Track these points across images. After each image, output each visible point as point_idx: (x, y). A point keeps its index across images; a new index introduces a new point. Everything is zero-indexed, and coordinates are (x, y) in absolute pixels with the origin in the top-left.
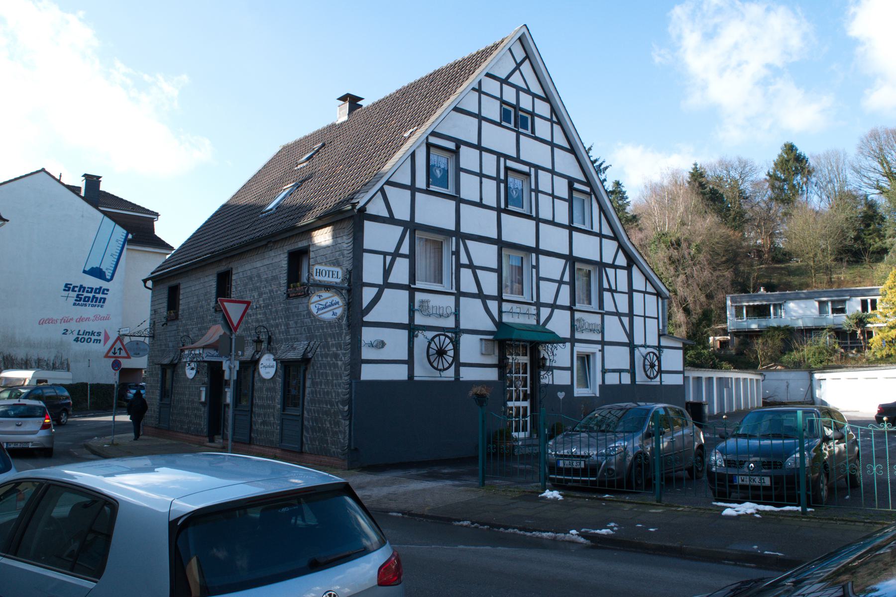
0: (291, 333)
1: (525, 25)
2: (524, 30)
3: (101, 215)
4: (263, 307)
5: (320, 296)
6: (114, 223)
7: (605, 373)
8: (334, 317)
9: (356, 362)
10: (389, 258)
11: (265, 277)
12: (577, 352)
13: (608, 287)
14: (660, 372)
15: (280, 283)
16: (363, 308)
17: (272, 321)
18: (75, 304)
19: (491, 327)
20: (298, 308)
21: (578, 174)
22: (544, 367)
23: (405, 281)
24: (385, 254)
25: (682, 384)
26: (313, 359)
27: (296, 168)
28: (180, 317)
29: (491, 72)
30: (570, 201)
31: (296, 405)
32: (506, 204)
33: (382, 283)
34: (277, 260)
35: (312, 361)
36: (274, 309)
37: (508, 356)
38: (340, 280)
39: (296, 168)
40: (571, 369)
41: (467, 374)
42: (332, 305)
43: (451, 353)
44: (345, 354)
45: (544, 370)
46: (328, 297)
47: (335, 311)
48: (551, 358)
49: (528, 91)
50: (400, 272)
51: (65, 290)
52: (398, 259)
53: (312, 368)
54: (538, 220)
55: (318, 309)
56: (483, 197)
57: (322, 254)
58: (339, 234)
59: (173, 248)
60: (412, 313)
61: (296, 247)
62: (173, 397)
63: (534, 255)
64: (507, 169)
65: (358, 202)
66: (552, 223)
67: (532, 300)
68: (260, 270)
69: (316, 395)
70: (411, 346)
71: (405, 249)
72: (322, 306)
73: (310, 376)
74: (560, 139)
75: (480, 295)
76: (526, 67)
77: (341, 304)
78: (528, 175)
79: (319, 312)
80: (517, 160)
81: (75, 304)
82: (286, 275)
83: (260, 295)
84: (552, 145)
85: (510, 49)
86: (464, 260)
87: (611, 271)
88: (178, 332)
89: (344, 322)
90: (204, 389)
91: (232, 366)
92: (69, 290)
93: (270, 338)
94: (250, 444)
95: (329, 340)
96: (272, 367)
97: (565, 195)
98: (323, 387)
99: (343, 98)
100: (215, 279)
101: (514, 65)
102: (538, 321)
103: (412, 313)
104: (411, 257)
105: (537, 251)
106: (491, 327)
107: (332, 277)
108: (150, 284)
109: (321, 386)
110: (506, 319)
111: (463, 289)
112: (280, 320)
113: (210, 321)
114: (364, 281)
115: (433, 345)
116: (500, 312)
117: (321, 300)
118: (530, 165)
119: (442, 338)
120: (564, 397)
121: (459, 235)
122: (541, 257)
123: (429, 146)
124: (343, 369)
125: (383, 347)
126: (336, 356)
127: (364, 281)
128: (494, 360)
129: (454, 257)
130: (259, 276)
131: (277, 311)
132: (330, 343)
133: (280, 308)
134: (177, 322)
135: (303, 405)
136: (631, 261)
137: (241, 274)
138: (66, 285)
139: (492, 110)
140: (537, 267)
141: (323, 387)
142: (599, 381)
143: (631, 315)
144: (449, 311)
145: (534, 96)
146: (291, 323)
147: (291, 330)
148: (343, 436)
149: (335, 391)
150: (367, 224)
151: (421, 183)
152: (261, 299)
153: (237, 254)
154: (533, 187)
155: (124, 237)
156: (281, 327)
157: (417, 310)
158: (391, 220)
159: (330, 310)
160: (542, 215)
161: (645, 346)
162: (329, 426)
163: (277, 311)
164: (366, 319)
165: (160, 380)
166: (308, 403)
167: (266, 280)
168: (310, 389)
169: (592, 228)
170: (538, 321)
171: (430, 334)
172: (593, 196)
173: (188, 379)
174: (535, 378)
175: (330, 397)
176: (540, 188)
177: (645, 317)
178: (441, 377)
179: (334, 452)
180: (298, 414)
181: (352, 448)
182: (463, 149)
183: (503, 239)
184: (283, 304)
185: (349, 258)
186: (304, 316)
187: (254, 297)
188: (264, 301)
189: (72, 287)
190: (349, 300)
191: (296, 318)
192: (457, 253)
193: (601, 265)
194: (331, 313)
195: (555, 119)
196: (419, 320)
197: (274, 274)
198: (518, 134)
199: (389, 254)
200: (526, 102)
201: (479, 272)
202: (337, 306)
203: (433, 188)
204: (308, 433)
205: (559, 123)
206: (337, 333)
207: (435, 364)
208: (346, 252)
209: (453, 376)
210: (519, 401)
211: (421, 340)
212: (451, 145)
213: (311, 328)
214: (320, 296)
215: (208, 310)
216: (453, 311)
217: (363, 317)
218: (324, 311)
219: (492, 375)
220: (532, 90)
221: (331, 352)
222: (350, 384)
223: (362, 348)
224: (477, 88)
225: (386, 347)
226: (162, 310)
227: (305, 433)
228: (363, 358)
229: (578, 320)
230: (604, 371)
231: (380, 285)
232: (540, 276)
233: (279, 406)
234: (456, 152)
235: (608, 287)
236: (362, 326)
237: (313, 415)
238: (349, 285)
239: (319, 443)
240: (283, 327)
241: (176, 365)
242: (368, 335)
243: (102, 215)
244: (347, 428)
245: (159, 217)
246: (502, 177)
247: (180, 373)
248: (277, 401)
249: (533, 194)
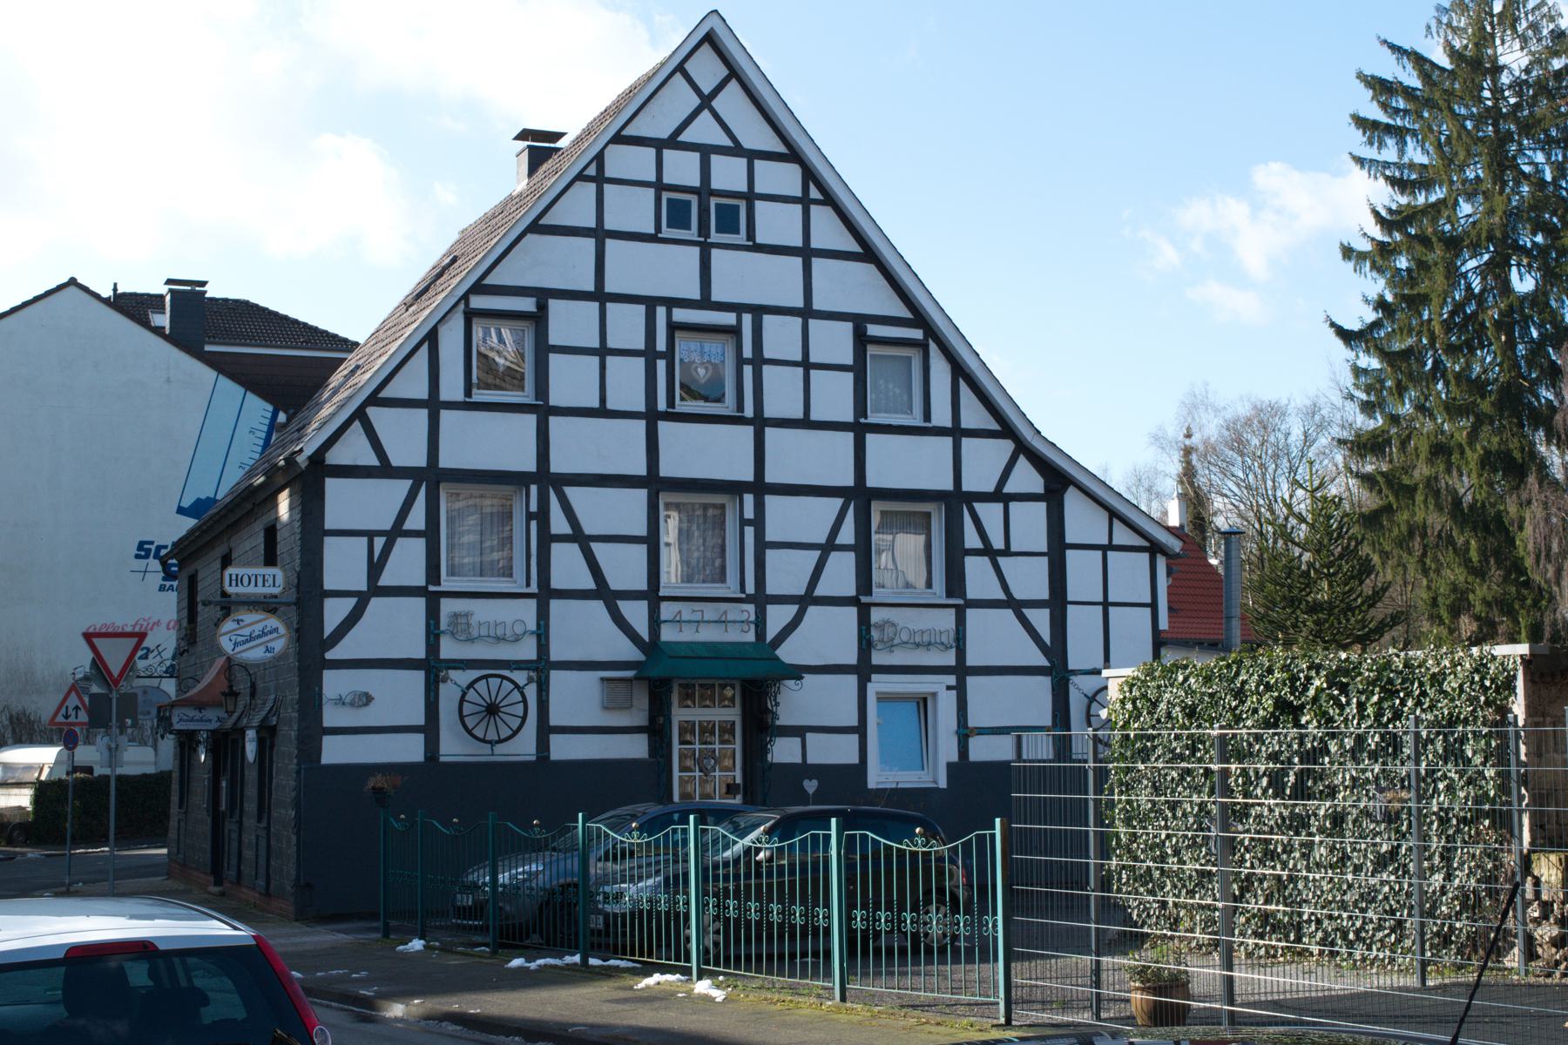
3: (209, 374)
6: (240, 390)
8: (268, 655)
9: (313, 731)
10: (379, 543)
12: (877, 693)
13: (978, 544)
18: (162, 588)
19: (629, 652)
23: (419, 579)
24: (370, 535)
30: (858, 369)
32: (671, 402)
41: (563, 749)
42: (264, 634)
46: (253, 621)
47: (269, 645)
49: (736, 150)
50: (407, 565)
51: (137, 556)
55: (236, 644)
60: (432, 639)
64: (673, 327)
65: (301, 450)
72: (244, 638)
75: (603, 592)
77: (282, 630)
78: (735, 331)
79: (237, 650)
81: (162, 588)
86: (559, 524)
87: (990, 514)
91: (113, 746)
92: (146, 557)
93: (253, 686)
103: (432, 639)
106: (627, 651)
107: (264, 585)
110: (668, 634)
111: (557, 582)
115: (471, 695)
116: (655, 622)
117: (241, 628)
118: (738, 308)
120: (817, 790)
121: (545, 479)
123: (470, 316)
125: (366, 704)
128: (639, 717)
129: (534, 524)
138: (141, 545)
140: (759, 522)
143: (1058, 601)
144: (519, 630)
145: (752, 156)
150: (331, 484)
151: (452, 388)
155: (267, 422)
158: (385, 470)
159: (261, 644)
164: (329, 655)
172: (933, 346)
177: (1106, 604)
189: (153, 548)
192: (543, 516)
194: (263, 648)
195: (814, 193)
196: (448, 649)
199: (380, 533)
201: (597, 548)
202: (275, 635)
203: (480, 396)
212: (527, 304)
214: (238, 622)
216: (532, 626)
217: (324, 653)
218: (248, 645)
220: (747, 144)
225: (372, 704)
229: (881, 627)
230: (965, 732)
234: (539, 319)
235: (978, 544)
242: (334, 684)
243: (211, 374)
246: (661, 345)
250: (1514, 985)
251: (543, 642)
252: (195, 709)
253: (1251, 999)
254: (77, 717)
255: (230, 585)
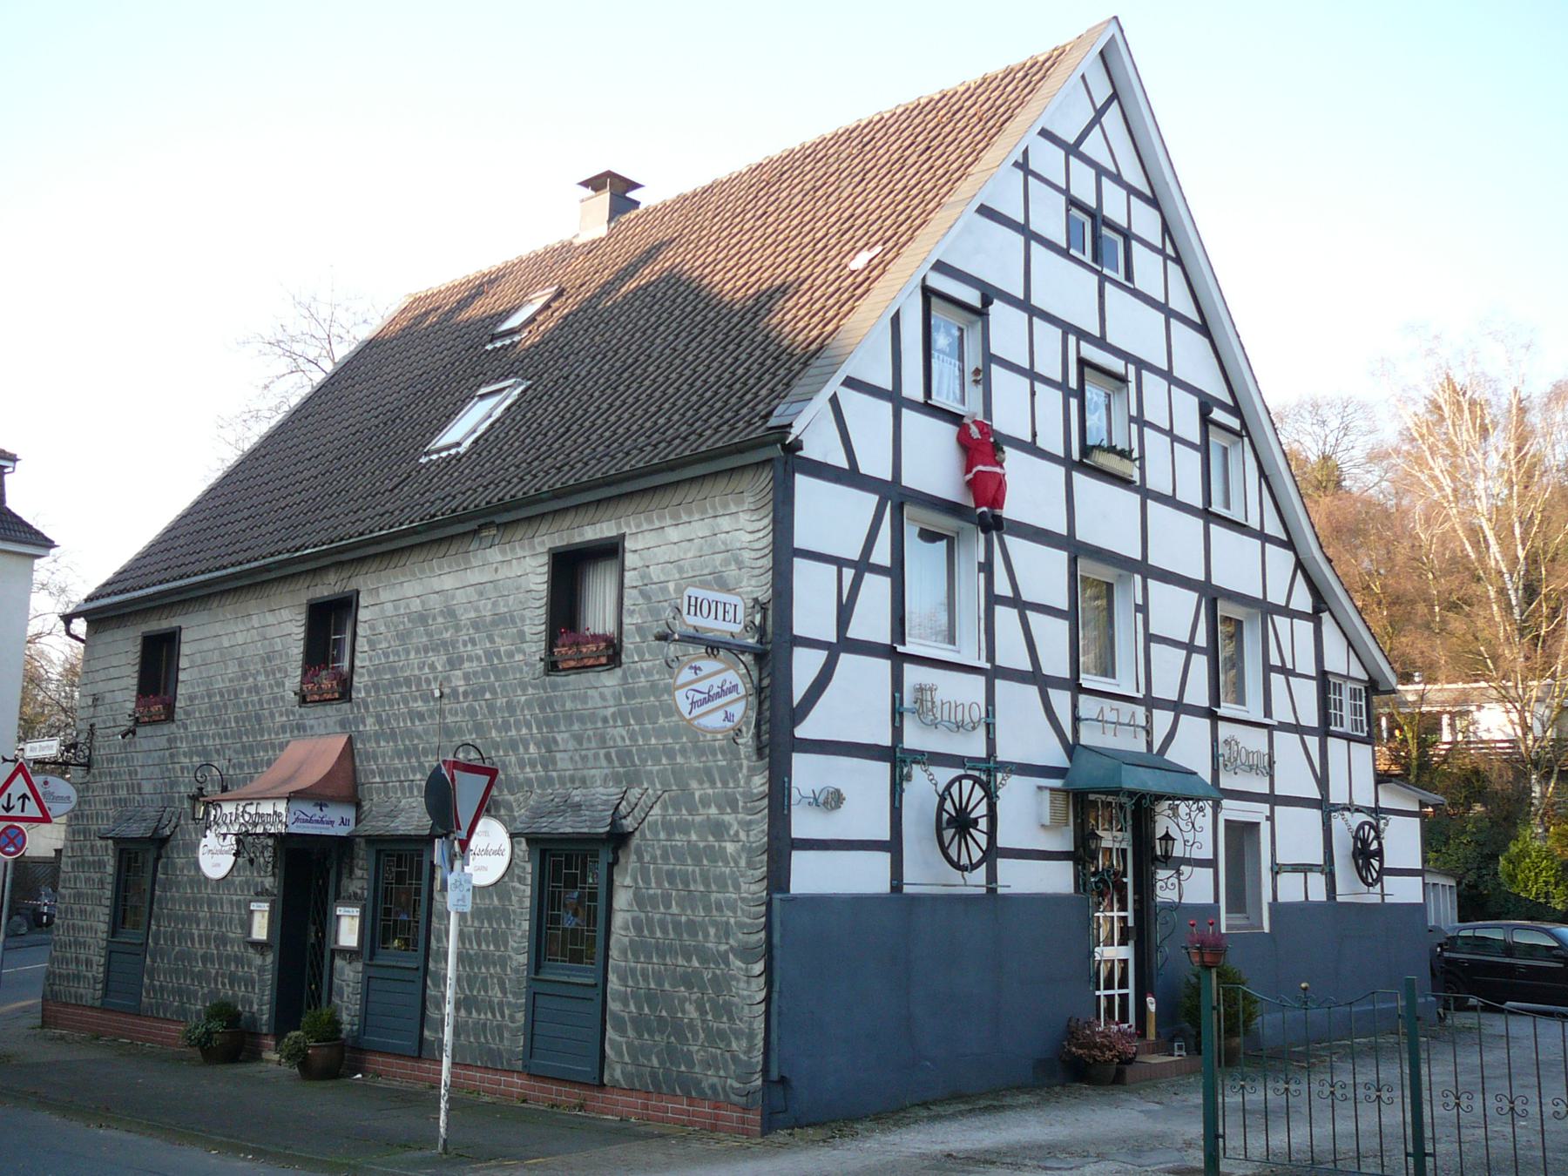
0: (560, 765)
1: (1116, 18)
2: (1113, 29)
4: (465, 694)
5: (696, 669)
7: (1277, 873)
8: (729, 724)
10: (848, 574)
11: (473, 615)
12: (1226, 820)
14: (993, 853)
15: (521, 634)
16: (795, 703)
17: (494, 733)
19: (1055, 756)
20: (584, 699)
21: (1218, 391)
22: (1167, 860)
24: (840, 563)
25: (1422, 901)
26: (637, 834)
27: (489, 347)
28: (179, 714)
29: (1049, 128)
30: (1204, 449)
31: (576, 957)
33: (834, 640)
34: (516, 569)
35: (635, 841)
36: (501, 702)
37: (1100, 833)
38: (742, 625)
39: (489, 347)
40: (1277, 870)
42: (723, 692)
43: (983, 824)
44: (750, 823)
45: (1167, 867)
47: (730, 709)
48: (1189, 836)
49: (1117, 179)
52: (868, 578)
53: (633, 857)
54: (1146, 494)
56: (1037, 429)
57: (667, 559)
58: (726, 506)
59: (52, 542)
61: (577, 540)
62: (154, 928)
63: (1138, 578)
64: (1083, 363)
66: (1171, 501)
67: (1138, 691)
68: (453, 597)
69: (652, 932)
70: (897, 804)
71: (882, 554)
72: (702, 696)
73: (628, 881)
74: (1181, 302)
76: (1112, 117)
80: (1101, 342)
82: (543, 610)
83: (455, 663)
84: (1169, 313)
85: (1083, 77)
87: (1282, 622)
88: (172, 756)
89: (747, 739)
90: (266, 906)
94: (419, 1057)
95: (694, 784)
96: (498, 852)
97: (1196, 438)
98: (675, 909)
99: (595, 184)
100: (302, 618)
101: (1092, 114)
102: (1149, 744)
104: (896, 572)
105: (1144, 569)
108: (80, 626)
109: (668, 906)
110: (1088, 737)
112: (524, 731)
113: (283, 728)
114: (797, 631)
116: (1076, 719)
118: (1127, 357)
119: (967, 784)
122: (1152, 584)
123: (928, 293)
124: (743, 863)
126: (719, 829)
127: (797, 631)
128: (1063, 841)
130: (450, 613)
131: (510, 707)
132: (697, 794)
133: (523, 698)
134: (166, 729)
135: (607, 957)
136: (1321, 602)
137: (389, 606)
139: (1050, 219)
140: (1143, 609)
141: (675, 909)
142: (1267, 897)
145: (1132, 191)
146: (559, 737)
147: (559, 755)
148: (744, 1043)
149: (715, 924)
152: (458, 673)
153: (376, 555)
154: (1134, 412)
156: (526, 749)
157: (909, 710)
158: (851, 477)
160: (1152, 483)
161: (1350, 808)
162: (695, 1015)
163: (510, 707)
164: (801, 732)
165: (109, 879)
166: (624, 953)
167: (476, 625)
168: (628, 916)
169: (1247, 520)
170: (1149, 744)
171: (945, 775)
173: (206, 878)
174: (1145, 886)
175: (700, 937)
176: (1148, 417)
178: (966, 885)
179: (713, 1087)
180: (415, 966)
181: (774, 1075)
182: (997, 309)
183: (1078, 538)
184: (534, 687)
185: (757, 572)
186: (605, 720)
187: (432, 667)
188: (466, 677)
190: (760, 680)
191: (576, 727)
192: (987, 568)
193: (1266, 609)
194: (721, 714)
195: (1170, 250)
196: (914, 738)
197: (503, 610)
198: (1103, 279)
200: (1115, 205)
201: (1032, 616)
202: (734, 696)
204: (623, 1032)
205: (1178, 260)
206: (720, 768)
207: (953, 852)
208: (746, 555)
209: (984, 883)
210: (1113, 945)
211: (923, 786)
212: (972, 297)
213: (629, 753)
214: (696, 669)
215: (275, 699)
219: (1057, 879)
221: (698, 819)
222: (769, 904)
223: (793, 808)
224: (1021, 161)
226: (119, 696)
227: (610, 1033)
228: (794, 835)
231: (831, 643)
232: (1151, 631)
233: (523, 959)
234: (981, 313)
236: (793, 751)
237: (642, 984)
238: (760, 641)
239: (662, 1062)
240: (532, 749)
241: (164, 841)
242: (807, 772)
244: (759, 1025)
245: (18, 463)
247: (180, 862)
248: (512, 943)
249: (1134, 427)
250: (1193, 1073)
251: (991, 736)
252: (316, 805)
253: (1428, 1133)
254: (23, 811)
255: (689, 613)
